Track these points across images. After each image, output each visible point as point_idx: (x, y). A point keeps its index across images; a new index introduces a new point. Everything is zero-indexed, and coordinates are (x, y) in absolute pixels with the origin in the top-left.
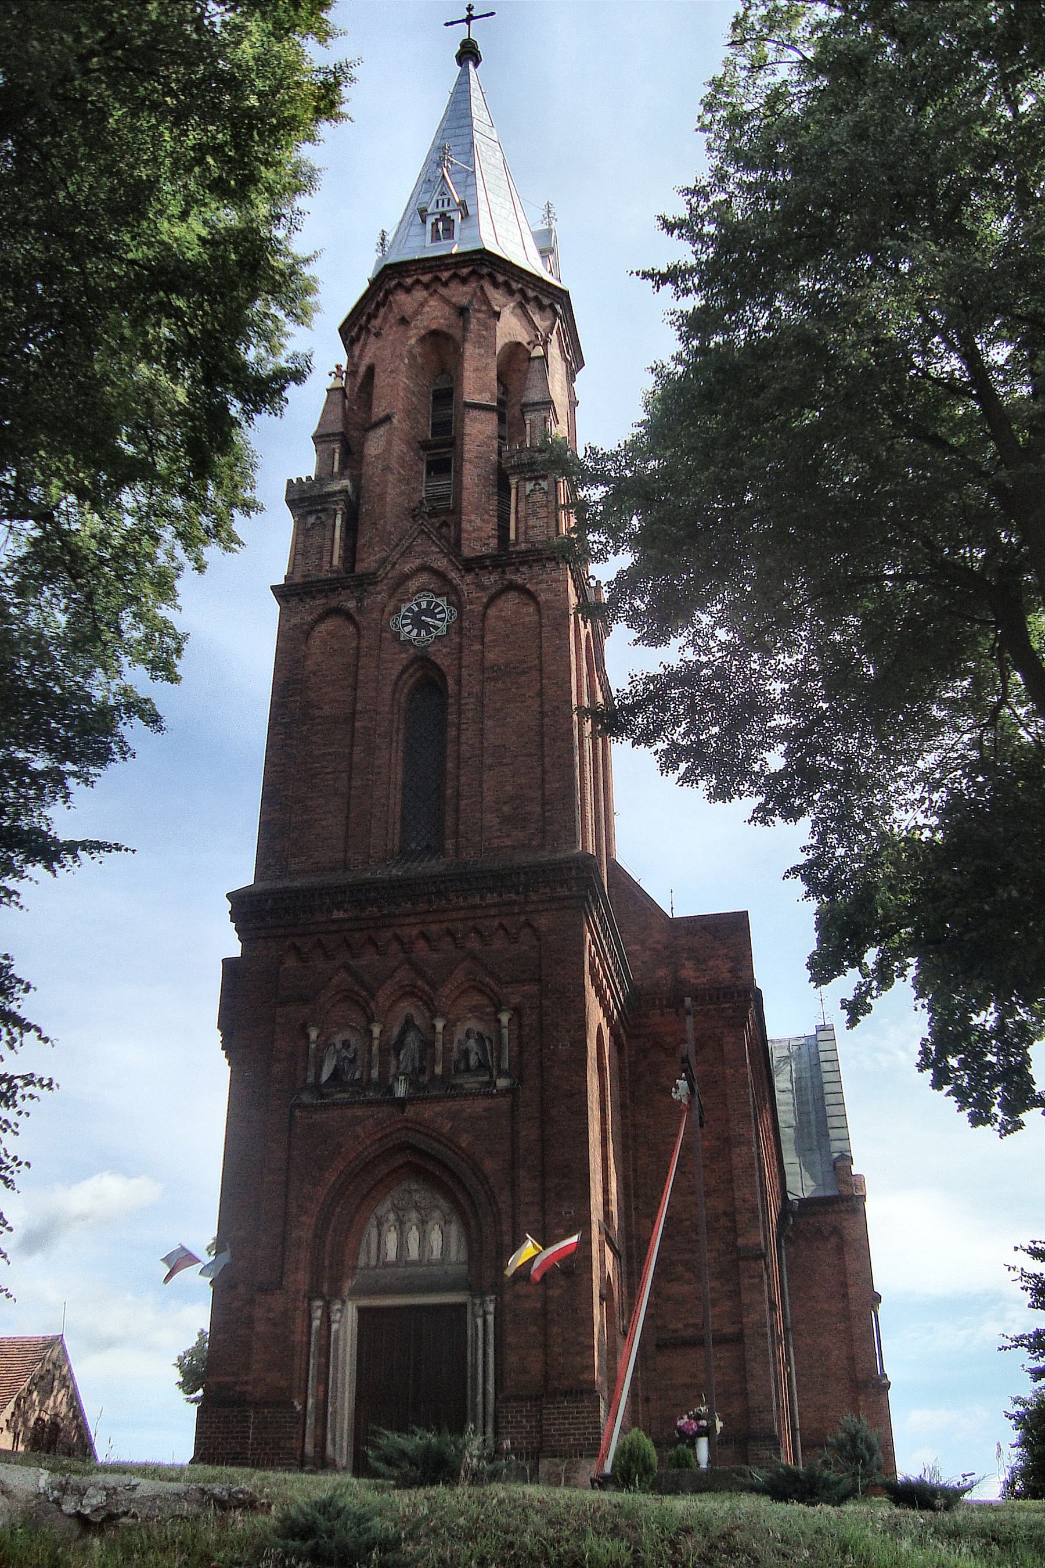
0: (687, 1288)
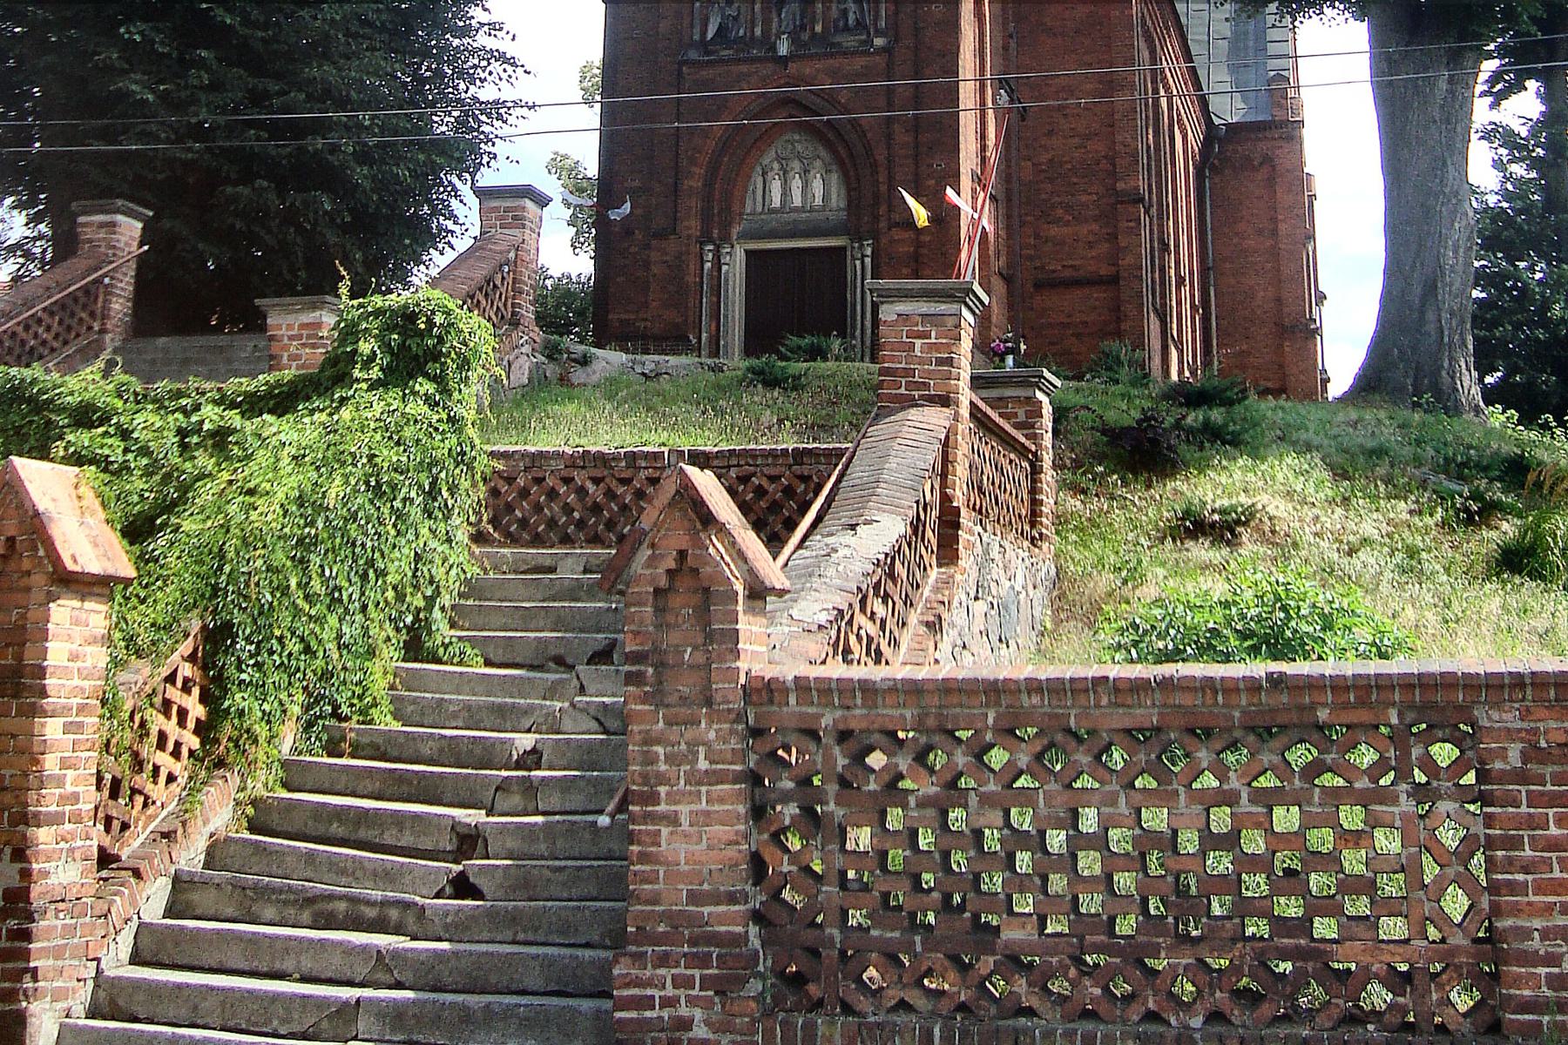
0: (1065, 230)
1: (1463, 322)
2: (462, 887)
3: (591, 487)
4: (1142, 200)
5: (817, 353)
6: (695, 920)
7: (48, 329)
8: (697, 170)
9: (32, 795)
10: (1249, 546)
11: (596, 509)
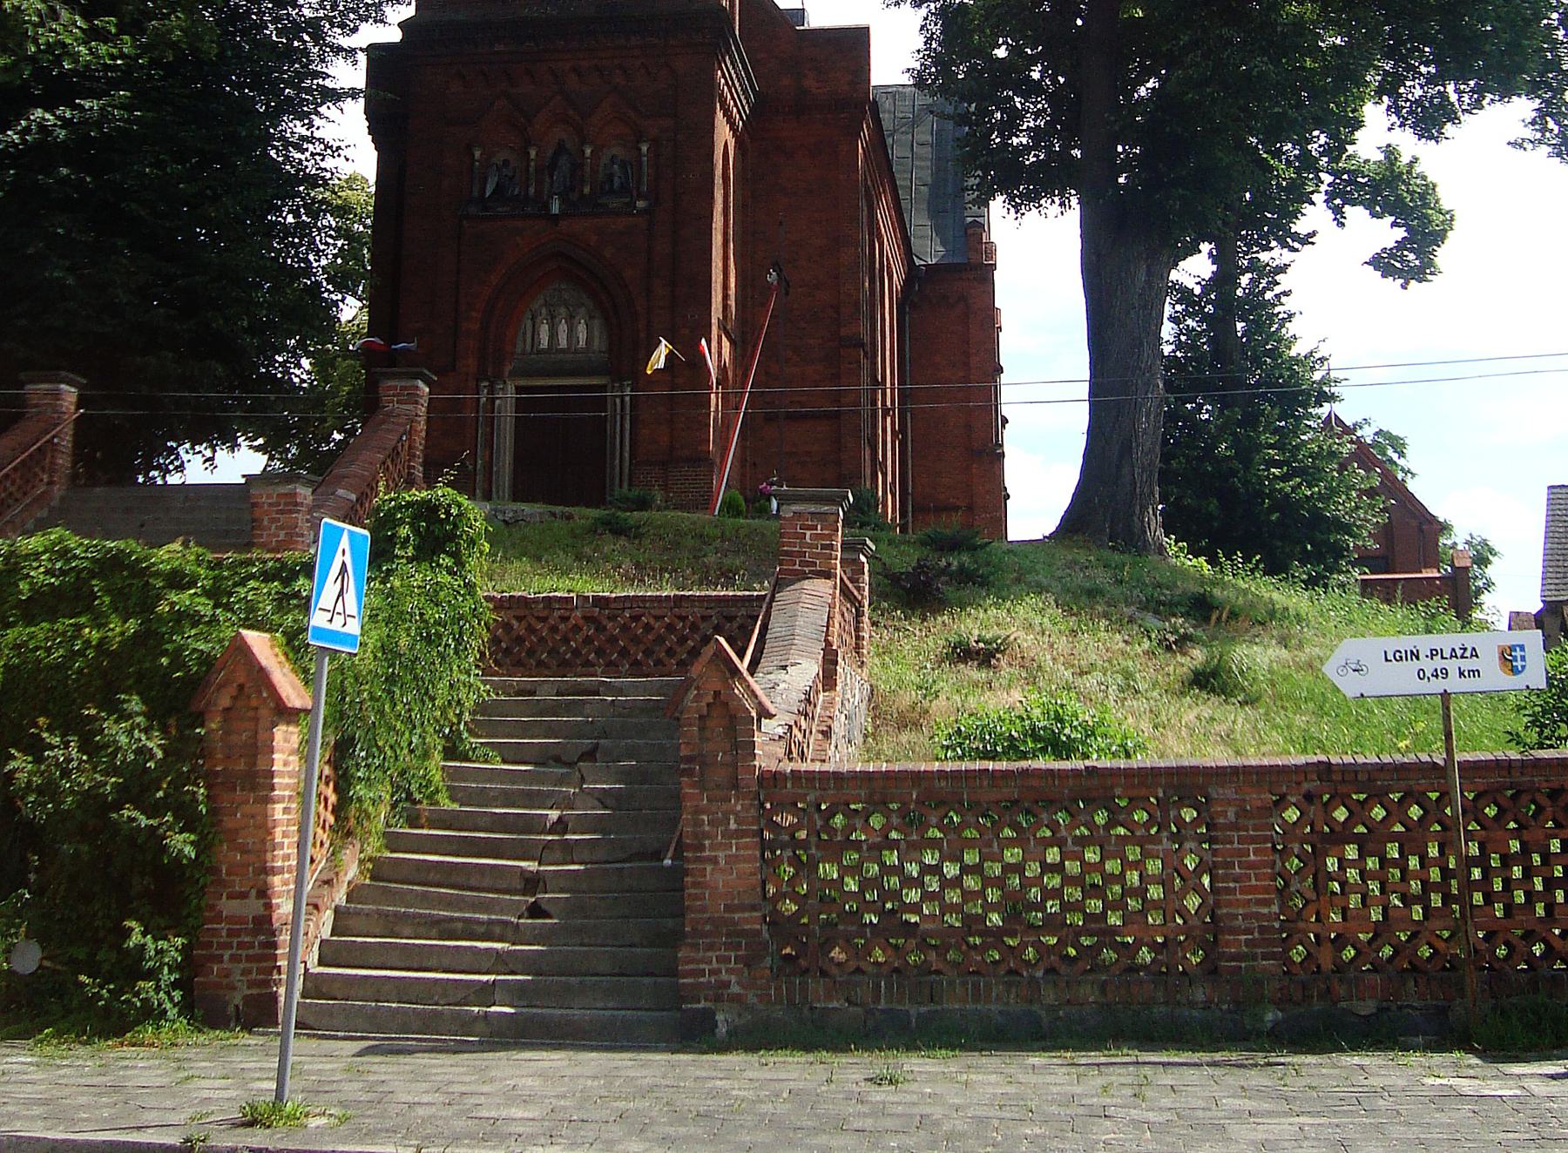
1: (1150, 476)
2: (536, 911)
3: (515, 624)
4: (863, 345)
5: (643, 504)
6: (733, 922)
7: (13, 483)
8: (474, 314)
9: (269, 855)
10: (1006, 668)
11: (519, 640)
